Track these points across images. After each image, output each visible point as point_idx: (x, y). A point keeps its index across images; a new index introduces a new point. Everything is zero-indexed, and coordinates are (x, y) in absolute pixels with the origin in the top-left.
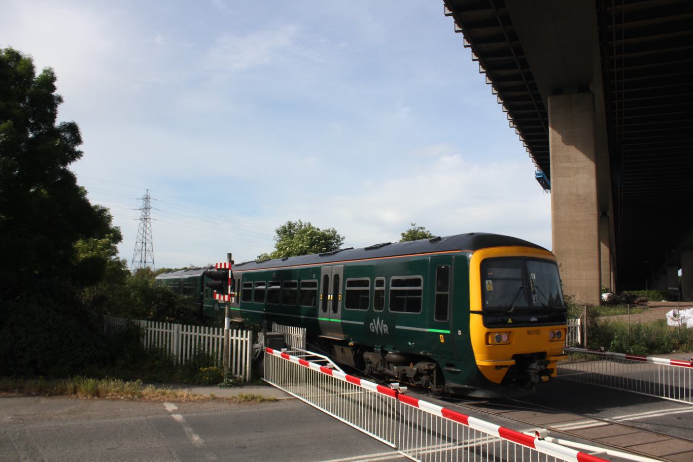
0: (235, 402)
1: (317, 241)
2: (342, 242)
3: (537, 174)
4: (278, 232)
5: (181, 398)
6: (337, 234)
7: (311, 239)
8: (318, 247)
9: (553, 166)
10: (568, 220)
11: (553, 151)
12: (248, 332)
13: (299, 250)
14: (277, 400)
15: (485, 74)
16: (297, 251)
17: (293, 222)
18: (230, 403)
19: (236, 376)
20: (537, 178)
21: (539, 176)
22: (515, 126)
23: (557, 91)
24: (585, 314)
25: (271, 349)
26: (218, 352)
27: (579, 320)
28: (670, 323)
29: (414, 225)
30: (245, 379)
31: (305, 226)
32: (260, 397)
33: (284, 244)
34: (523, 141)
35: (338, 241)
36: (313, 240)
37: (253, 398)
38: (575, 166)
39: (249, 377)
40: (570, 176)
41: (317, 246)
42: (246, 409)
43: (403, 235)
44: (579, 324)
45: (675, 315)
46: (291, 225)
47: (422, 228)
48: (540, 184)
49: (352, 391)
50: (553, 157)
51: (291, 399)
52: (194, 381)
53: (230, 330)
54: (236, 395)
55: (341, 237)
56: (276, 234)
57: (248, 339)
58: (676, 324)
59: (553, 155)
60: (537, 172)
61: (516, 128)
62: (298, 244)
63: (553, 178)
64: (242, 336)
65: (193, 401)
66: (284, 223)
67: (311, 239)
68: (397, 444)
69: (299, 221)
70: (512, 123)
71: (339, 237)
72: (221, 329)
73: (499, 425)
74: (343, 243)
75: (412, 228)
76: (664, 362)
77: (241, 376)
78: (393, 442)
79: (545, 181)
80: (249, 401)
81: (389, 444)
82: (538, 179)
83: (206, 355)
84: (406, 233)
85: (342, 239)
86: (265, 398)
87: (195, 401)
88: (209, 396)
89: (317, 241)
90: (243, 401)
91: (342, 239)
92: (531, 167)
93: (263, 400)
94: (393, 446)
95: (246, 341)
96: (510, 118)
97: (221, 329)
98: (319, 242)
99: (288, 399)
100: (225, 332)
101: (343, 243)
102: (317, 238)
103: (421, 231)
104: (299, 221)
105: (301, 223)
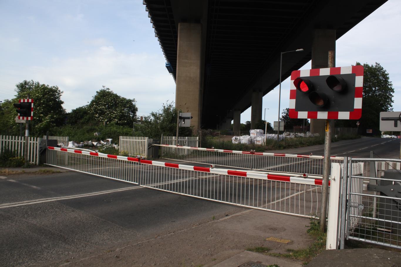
0: (37, 174)
1: (48, 92)
2: (61, 94)
3: (167, 64)
4: (18, 86)
5: (5, 173)
6: (59, 89)
7: (44, 91)
8: (48, 97)
9: (179, 61)
10: (184, 90)
11: (179, 53)
12: (38, 138)
13: (36, 98)
14: (61, 172)
15: (146, 5)
16: (35, 98)
17: (28, 81)
18: (36, 174)
19: (30, 162)
20: (166, 66)
21: (168, 66)
22: (158, 36)
23: (184, 20)
24: (201, 135)
25: (53, 147)
26: (18, 150)
27: (198, 137)
28: (233, 142)
29: (104, 87)
30: (36, 164)
31: (36, 83)
32: (52, 171)
33: (26, 94)
34: (161, 45)
35: (59, 94)
36: (45, 92)
37: (48, 171)
38: (190, 62)
39: (38, 163)
40: (187, 67)
41: (48, 96)
42: (46, 176)
43: (97, 92)
44: (198, 139)
45: (236, 139)
46: (26, 83)
47: (108, 89)
48: (168, 70)
49: (100, 167)
50: (179, 56)
51: (68, 172)
52: (6, 166)
53: (29, 138)
54: (38, 171)
55: (61, 91)
56: (16, 88)
57: (38, 142)
58: (237, 143)
59: (179, 55)
60: (167, 63)
61: (158, 37)
62: (35, 94)
63: (178, 67)
64: (34, 141)
65: (12, 174)
66: (22, 81)
67: (44, 91)
68: (139, 183)
69: (32, 80)
70: (156, 35)
71: (59, 91)
72: (23, 137)
73: (193, 166)
74: (61, 95)
75: (103, 88)
76: (239, 153)
77: (33, 163)
78: (137, 182)
79: (172, 68)
80: (46, 173)
81: (135, 183)
82: (167, 67)
83: (10, 151)
84: (99, 91)
85: (62, 92)
86: (55, 171)
87: (14, 174)
88: (21, 172)
89: (48, 92)
90: (43, 173)
91: (62, 92)
92: (163, 61)
93: (53, 173)
94: (137, 184)
95: (37, 143)
96: (156, 32)
97: (23, 137)
98: (48, 94)
99: (66, 172)
100: (26, 138)
101: (61, 95)
102: (47, 91)
103: (107, 90)
104: (32, 80)
105: (33, 82)
